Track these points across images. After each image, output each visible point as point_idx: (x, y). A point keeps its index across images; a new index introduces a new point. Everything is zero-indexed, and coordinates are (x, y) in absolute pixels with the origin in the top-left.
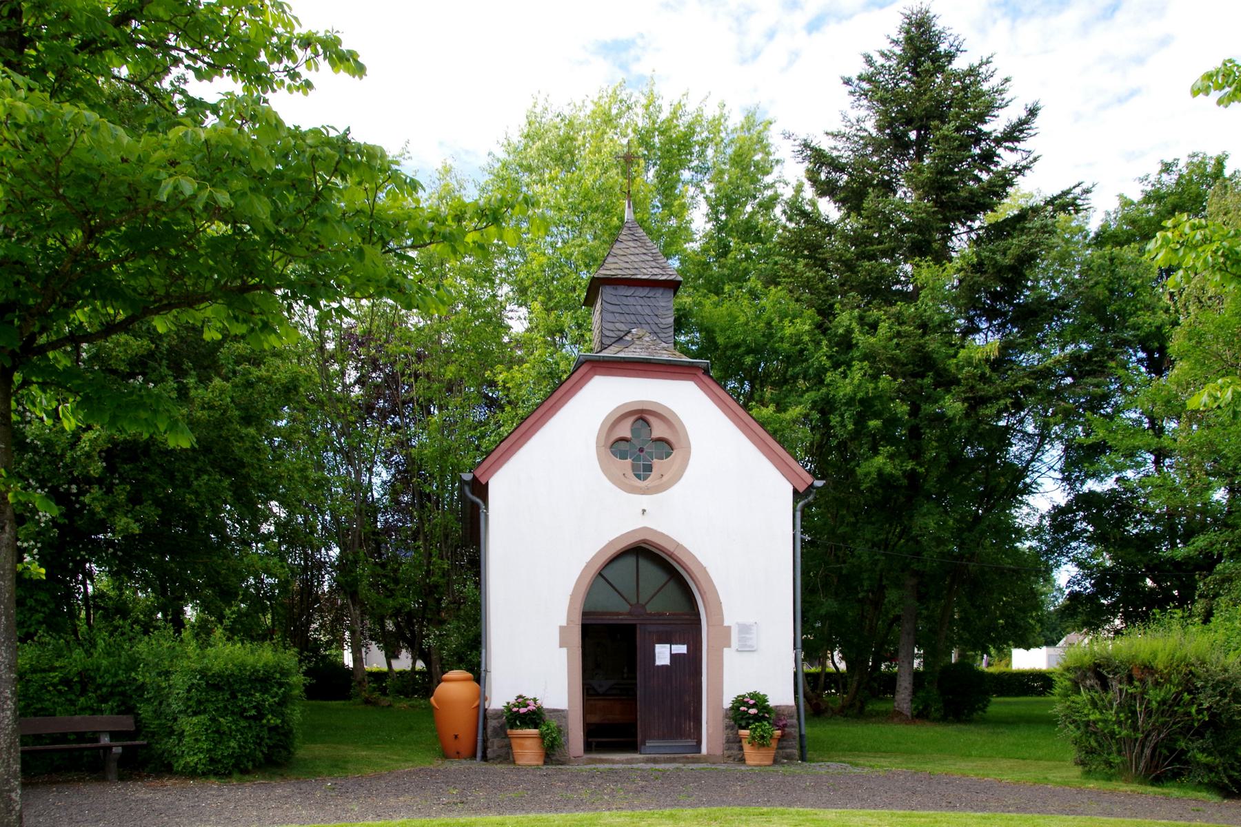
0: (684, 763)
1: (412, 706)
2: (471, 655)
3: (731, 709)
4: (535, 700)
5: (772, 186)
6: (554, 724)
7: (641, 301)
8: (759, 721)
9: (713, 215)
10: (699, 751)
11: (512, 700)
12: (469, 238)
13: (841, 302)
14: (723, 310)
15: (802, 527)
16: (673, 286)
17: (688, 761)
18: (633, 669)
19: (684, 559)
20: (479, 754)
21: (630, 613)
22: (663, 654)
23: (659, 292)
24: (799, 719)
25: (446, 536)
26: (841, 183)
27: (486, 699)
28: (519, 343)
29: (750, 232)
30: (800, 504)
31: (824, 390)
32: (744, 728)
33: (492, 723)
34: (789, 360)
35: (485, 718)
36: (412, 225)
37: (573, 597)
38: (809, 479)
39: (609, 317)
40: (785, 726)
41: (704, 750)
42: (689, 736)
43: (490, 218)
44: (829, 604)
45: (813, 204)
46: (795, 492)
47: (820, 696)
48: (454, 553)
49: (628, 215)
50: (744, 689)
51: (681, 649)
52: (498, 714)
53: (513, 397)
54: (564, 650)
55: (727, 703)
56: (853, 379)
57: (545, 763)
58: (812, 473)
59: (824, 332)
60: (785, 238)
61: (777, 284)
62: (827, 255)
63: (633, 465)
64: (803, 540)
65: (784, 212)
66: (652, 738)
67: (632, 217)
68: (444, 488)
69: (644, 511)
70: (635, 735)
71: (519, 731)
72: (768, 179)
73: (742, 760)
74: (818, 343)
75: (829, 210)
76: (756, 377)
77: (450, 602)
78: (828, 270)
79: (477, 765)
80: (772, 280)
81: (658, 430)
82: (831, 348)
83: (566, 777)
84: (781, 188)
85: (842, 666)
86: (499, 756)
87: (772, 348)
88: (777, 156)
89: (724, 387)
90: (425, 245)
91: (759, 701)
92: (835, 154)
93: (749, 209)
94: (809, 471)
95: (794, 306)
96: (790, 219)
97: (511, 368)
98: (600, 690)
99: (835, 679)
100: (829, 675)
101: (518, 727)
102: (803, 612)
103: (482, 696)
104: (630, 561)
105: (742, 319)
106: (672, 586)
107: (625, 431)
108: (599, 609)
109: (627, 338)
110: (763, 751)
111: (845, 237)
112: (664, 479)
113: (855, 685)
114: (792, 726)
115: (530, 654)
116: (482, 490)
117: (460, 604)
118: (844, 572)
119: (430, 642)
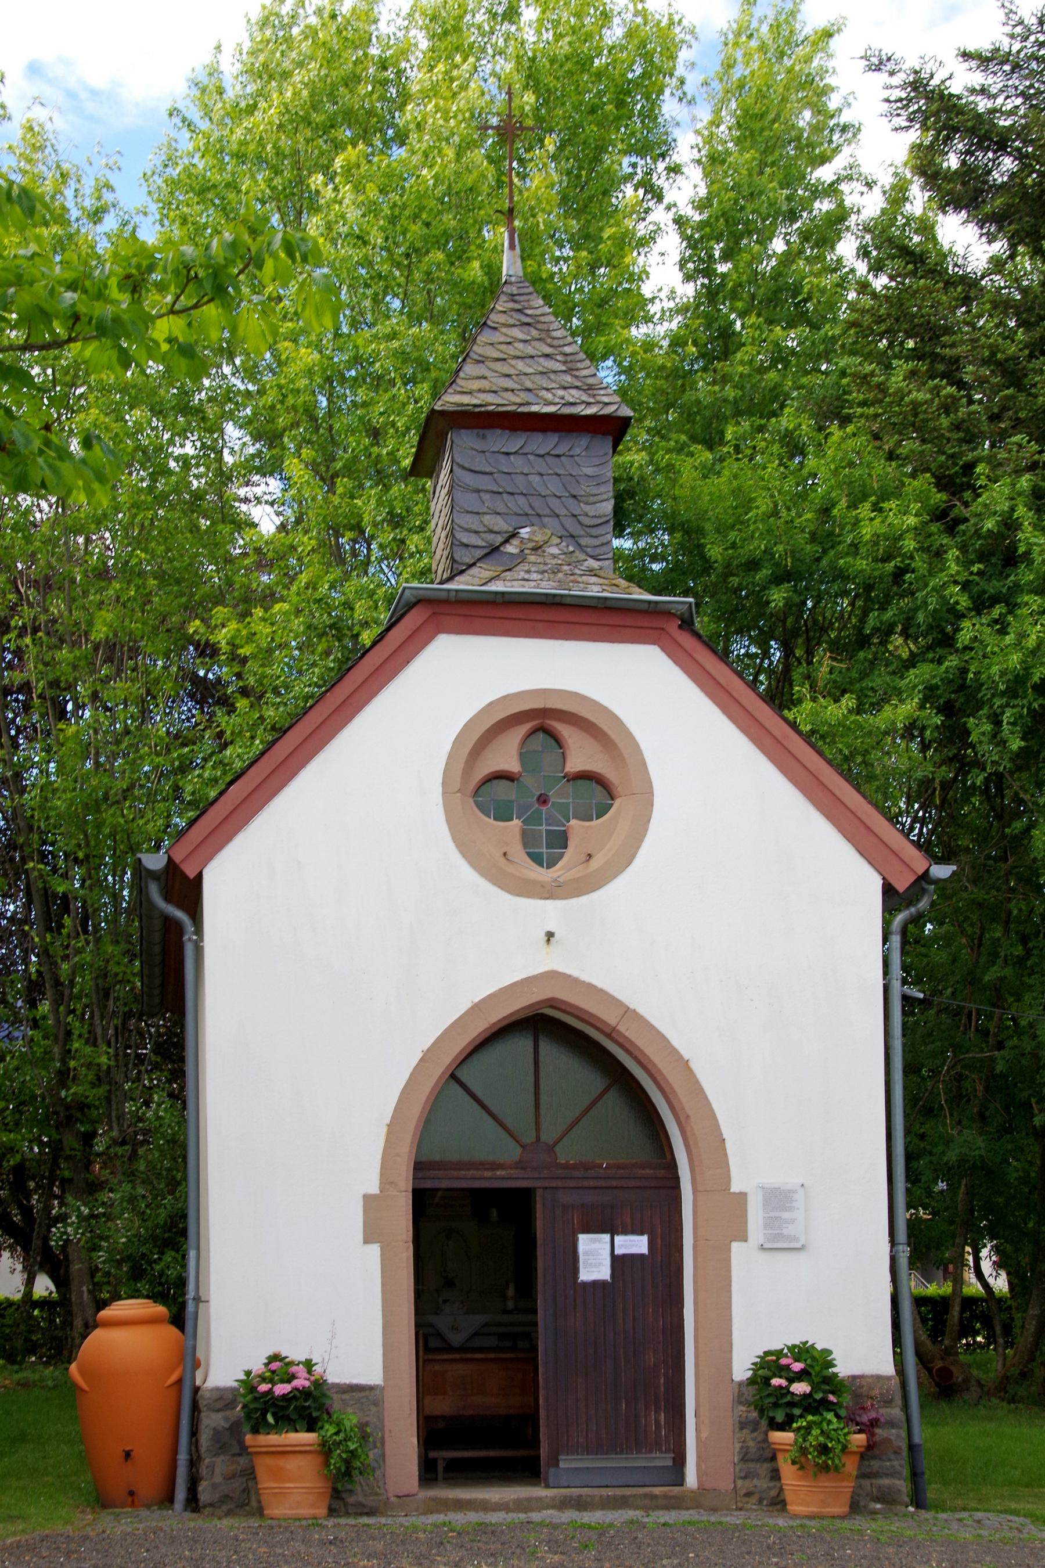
0: (647, 1509)
1: (24, 1385)
2: (163, 1264)
3: (751, 1381)
4: (309, 1364)
5: (831, 190)
6: (351, 1419)
7: (540, 465)
8: (815, 1411)
9: (697, 265)
10: (680, 1480)
11: (257, 1366)
12: (162, 329)
13: (990, 460)
14: (721, 483)
15: (905, 968)
16: (612, 429)
17: (653, 1504)
18: (526, 1287)
19: (641, 1042)
20: (181, 1494)
21: (518, 1165)
22: (595, 1257)
23: (580, 444)
24: (906, 1406)
25: (105, 994)
26: (998, 177)
27: (197, 1364)
28: (264, 557)
29: (781, 299)
30: (900, 918)
31: (952, 662)
32: (781, 1427)
33: (212, 1421)
34: (870, 594)
35: (195, 1407)
36: (25, 298)
37: (392, 1128)
38: (919, 862)
39: (469, 501)
40: (874, 1423)
41: (691, 1478)
42: (656, 1445)
43: (208, 286)
44: (967, 1142)
45: (926, 228)
46: (888, 890)
47: (950, 1352)
48: (122, 1030)
49: (509, 265)
50: (780, 1338)
51: (636, 1244)
52: (225, 1399)
53: (252, 681)
54: (375, 1249)
55: (741, 1369)
56: (1023, 636)
57: (332, 1512)
58: (924, 846)
59: (951, 529)
60: (863, 312)
61: (845, 421)
62: (961, 350)
63: (524, 834)
64: (905, 998)
65: (863, 252)
66: (573, 1449)
67: (518, 269)
68: (99, 884)
69: (550, 935)
70: (534, 1443)
71: (273, 1439)
72: (825, 174)
73: (779, 1503)
74: (939, 554)
75: (965, 242)
76: (795, 633)
77: (115, 1142)
78: (961, 385)
79: (176, 1519)
80: (833, 411)
81: (581, 755)
82: (967, 564)
83: (379, 1546)
84: (852, 194)
85: (1000, 1284)
86: (225, 1498)
87: (833, 566)
88: (844, 118)
89: (724, 656)
90: (58, 344)
91: (813, 1363)
92: (983, 105)
93: (778, 245)
94: (917, 845)
95: (882, 469)
96: (877, 268)
97: (247, 613)
98: (457, 1339)
99: (981, 1311)
100: (969, 1302)
101: (269, 1429)
102: (909, 1157)
103: (188, 1359)
104: (521, 1046)
105: (763, 505)
106: (614, 1104)
107: (505, 756)
108: (453, 1156)
109: (511, 549)
110: (826, 1482)
111: (1001, 305)
112: (595, 864)
113: (1032, 1327)
114: (891, 1424)
115: (297, 1260)
116: (188, 893)
117: (136, 1145)
118: (999, 1068)
119: (69, 1230)
